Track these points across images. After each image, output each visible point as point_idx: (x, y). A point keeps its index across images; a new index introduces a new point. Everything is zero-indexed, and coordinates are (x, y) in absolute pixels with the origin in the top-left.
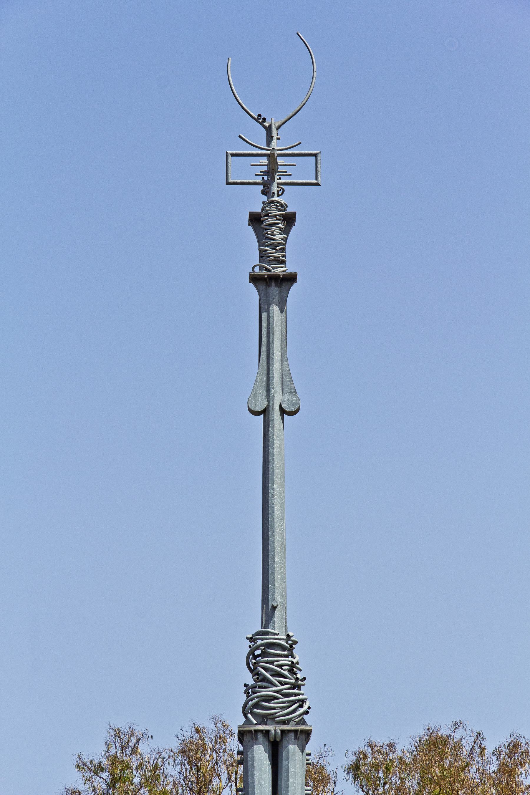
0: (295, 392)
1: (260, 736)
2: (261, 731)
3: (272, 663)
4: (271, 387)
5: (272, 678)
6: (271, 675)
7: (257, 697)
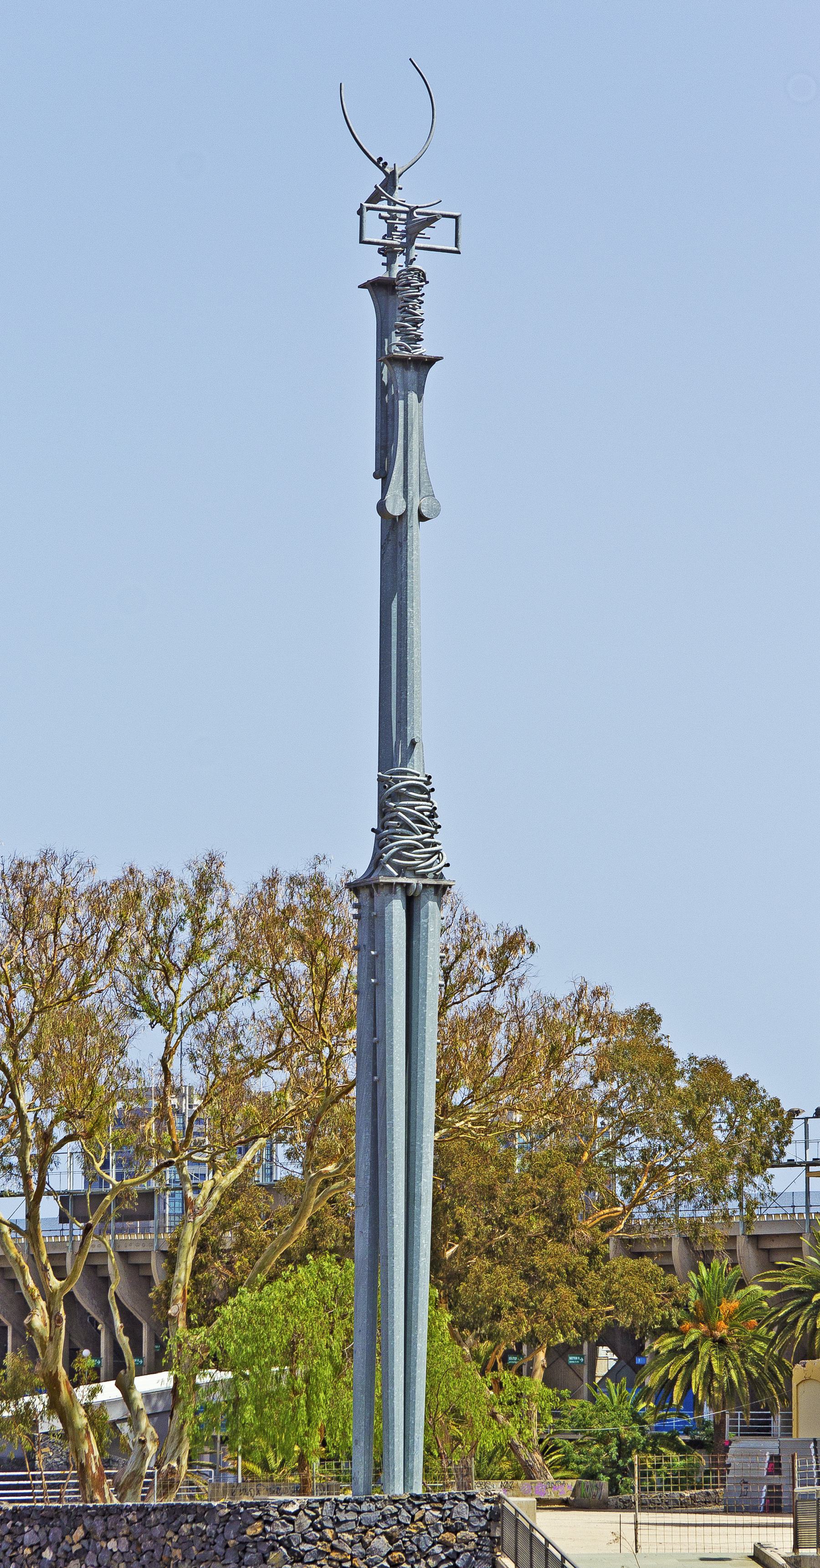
0: (433, 496)
1: (399, 889)
2: (401, 884)
3: (412, 807)
4: (409, 488)
5: (414, 825)
6: (413, 821)
7: (397, 846)
